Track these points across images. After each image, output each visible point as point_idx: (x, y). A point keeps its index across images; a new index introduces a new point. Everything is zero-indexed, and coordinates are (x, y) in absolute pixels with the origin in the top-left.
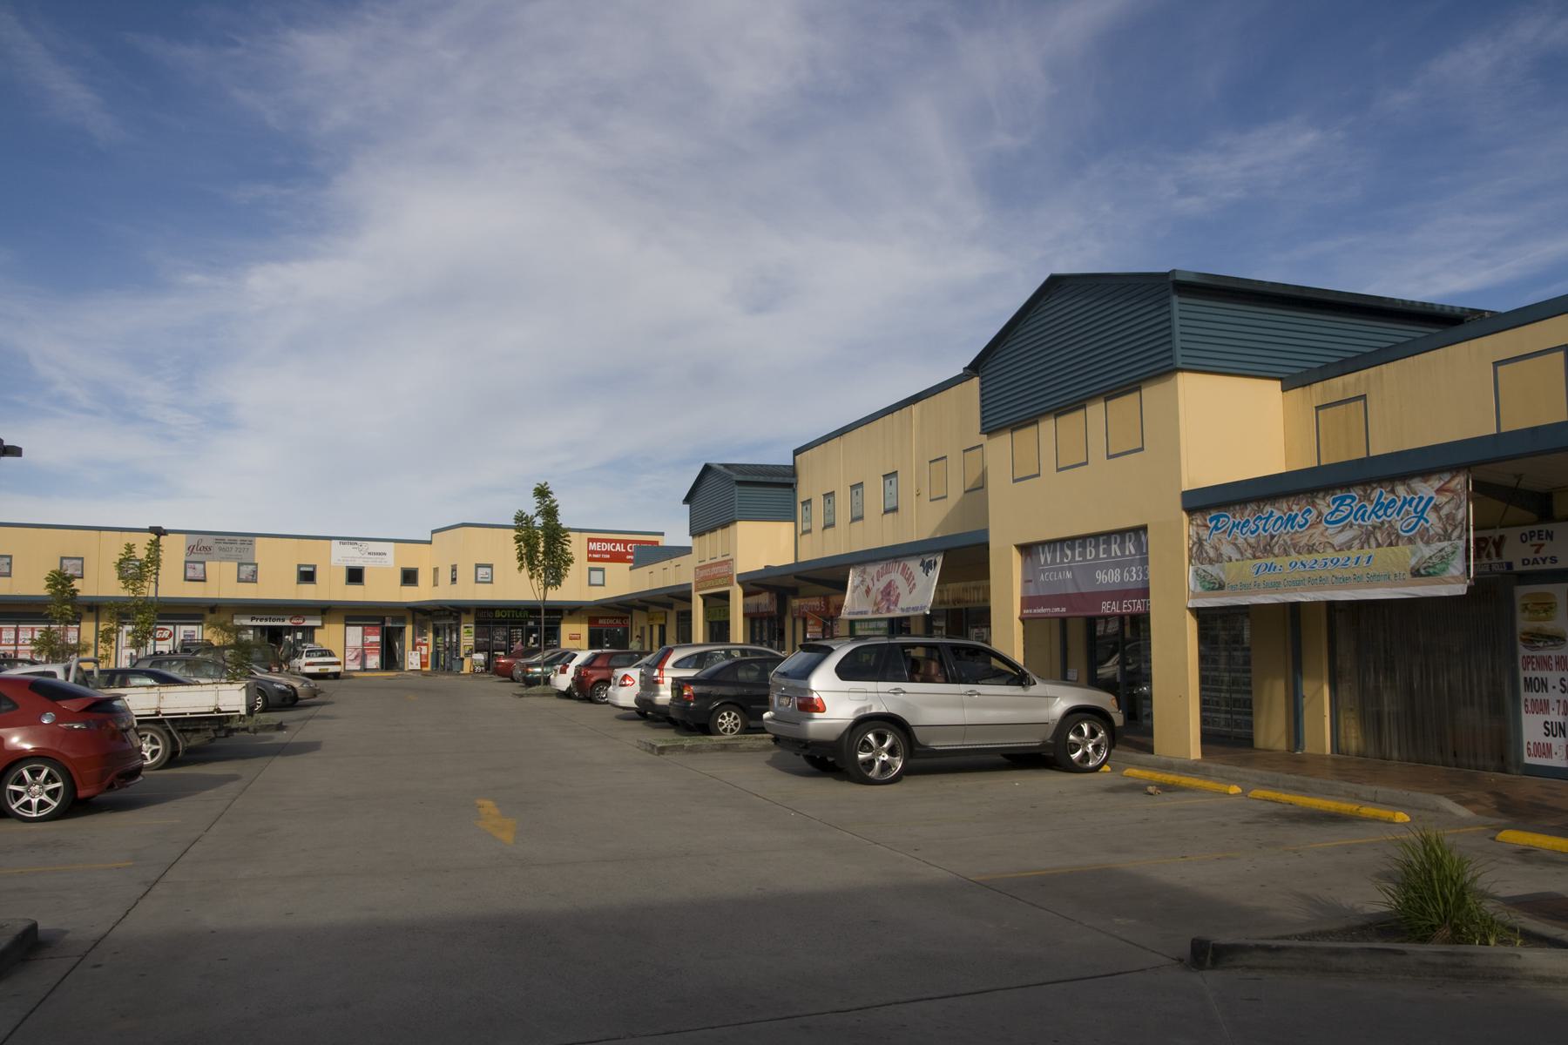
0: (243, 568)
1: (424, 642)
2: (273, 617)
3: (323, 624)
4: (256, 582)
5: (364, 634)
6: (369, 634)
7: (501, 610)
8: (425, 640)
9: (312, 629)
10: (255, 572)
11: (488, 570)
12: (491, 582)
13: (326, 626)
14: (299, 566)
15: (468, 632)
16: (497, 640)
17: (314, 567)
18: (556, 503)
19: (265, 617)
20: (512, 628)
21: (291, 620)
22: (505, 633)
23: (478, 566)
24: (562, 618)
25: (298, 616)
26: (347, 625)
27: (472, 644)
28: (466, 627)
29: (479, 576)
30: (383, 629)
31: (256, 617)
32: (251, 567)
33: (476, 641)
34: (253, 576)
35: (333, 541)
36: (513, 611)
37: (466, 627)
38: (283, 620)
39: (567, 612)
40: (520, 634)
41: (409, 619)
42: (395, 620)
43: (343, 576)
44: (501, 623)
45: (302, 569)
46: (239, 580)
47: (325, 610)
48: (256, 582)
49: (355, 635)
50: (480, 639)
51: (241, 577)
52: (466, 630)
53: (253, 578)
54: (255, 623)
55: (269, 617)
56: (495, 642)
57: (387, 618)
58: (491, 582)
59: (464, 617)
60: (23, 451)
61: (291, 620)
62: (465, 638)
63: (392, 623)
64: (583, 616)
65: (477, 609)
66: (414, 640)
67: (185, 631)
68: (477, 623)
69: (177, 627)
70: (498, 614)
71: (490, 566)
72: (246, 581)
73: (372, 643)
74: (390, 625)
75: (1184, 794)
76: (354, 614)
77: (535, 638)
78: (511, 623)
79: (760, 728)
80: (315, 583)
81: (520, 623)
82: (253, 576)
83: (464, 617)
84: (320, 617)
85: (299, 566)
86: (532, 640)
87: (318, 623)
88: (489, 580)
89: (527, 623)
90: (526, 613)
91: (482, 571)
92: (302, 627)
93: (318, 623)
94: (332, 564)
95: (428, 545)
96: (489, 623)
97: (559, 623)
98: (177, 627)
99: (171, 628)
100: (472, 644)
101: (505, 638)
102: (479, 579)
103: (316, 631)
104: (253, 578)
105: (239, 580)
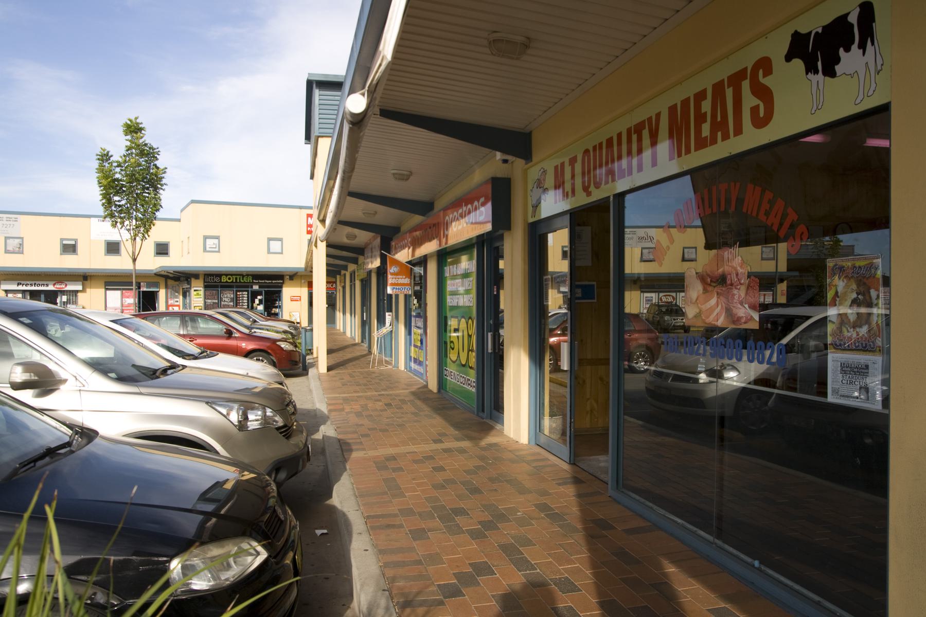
0: (10, 241)
1: (176, 303)
2: (37, 283)
3: (83, 288)
4: (23, 253)
5: (122, 296)
6: (208, 299)
7: (227, 275)
8: (177, 301)
9: (76, 292)
10: (21, 245)
11: (216, 241)
12: (219, 251)
13: (88, 290)
14: (62, 240)
15: (198, 294)
16: (225, 301)
17: (76, 241)
18: (102, 192)
19: (25, 282)
20: (240, 291)
21: (54, 285)
22: (232, 296)
23: (206, 238)
24: (283, 283)
25: (61, 282)
26: (107, 289)
27: (202, 305)
28: (195, 290)
29: (208, 247)
30: (139, 292)
31: (22, 282)
32: (17, 241)
33: (205, 302)
34: (19, 248)
35: (92, 219)
36: (238, 277)
37: (195, 290)
38: (47, 285)
39: (288, 277)
40: (246, 296)
41: (162, 283)
42: (149, 285)
43: (102, 248)
44: (227, 286)
45: (65, 242)
46: (7, 251)
47: (85, 277)
48: (23, 253)
49: (115, 297)
50: (209, 301)
51: (8, 249)
52: (195, 293)
53: (20, 250)
54: (21, 288)
55: (33, 283)
56: (223, 303)
57: (142, 284)
58: (219, 251)
59: (194, 282)
60: (729, 140)
61: (54, 285)
62: (195, 300)
63: (147, 288)
64: (303, 281)
65: (205, 275)
66: (167, 302)
67: (646, 297)
68: (206, 287)
69: (678, 294)
70: (224, 279)
71: (218, 238)
72: (13, 252)
73: (129, 305)
74: (145, 289)
75: (140, 436)
76: (113, 281)
77: (259, 300)
78: (237, 287)
79: (553, 382)
80: (121, 255)
81: (248, 287)
82: (19, 248)
83: (194, 282)
84: (81, 283)
85: (62, 240)
86: (257, 301)
87: (80, 288)
88: (217, 249)
89: (252, 287)
90: (250, 279)
91: (210, 242)
92: (64, 291)
93: (80, 288)
94: (92, 238)
95: (178, 223)
96: (216, 287)
97: (281, 287)
98: (678, 294)
99: (674, 294)
100: (202, 305)
101: (232, 300)
102: (208, 249)
103: (79, 294)
104: (20, 250)
105: (7, 251)
